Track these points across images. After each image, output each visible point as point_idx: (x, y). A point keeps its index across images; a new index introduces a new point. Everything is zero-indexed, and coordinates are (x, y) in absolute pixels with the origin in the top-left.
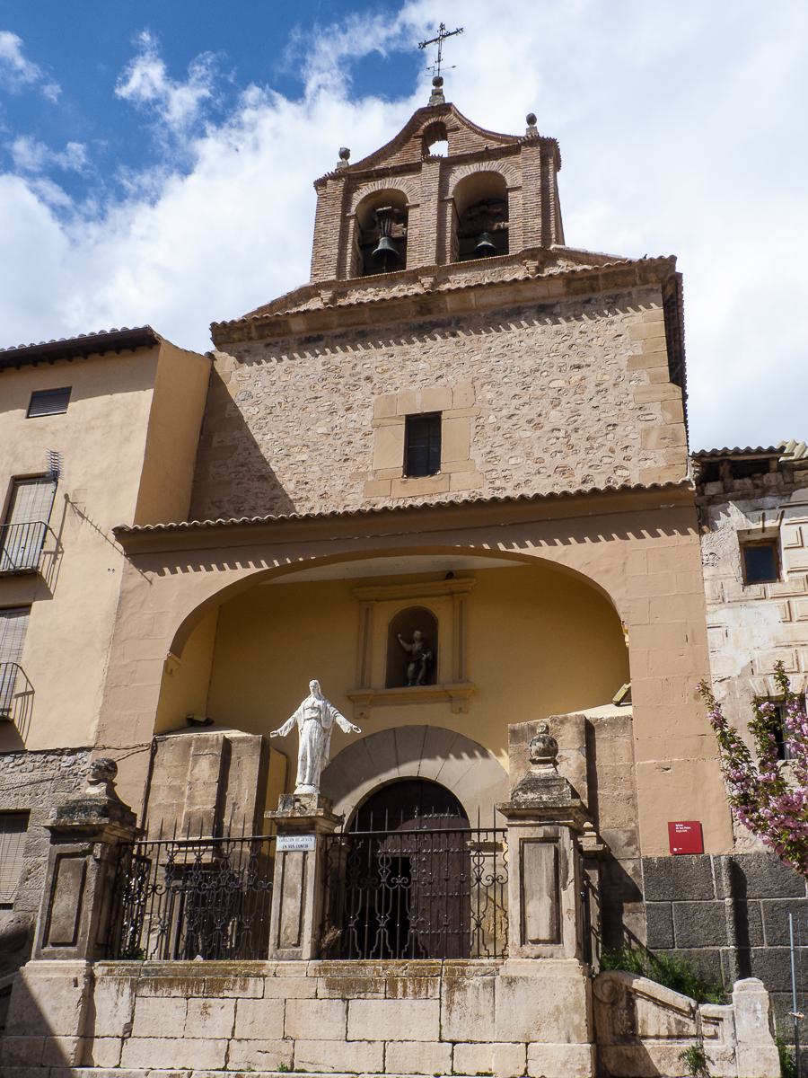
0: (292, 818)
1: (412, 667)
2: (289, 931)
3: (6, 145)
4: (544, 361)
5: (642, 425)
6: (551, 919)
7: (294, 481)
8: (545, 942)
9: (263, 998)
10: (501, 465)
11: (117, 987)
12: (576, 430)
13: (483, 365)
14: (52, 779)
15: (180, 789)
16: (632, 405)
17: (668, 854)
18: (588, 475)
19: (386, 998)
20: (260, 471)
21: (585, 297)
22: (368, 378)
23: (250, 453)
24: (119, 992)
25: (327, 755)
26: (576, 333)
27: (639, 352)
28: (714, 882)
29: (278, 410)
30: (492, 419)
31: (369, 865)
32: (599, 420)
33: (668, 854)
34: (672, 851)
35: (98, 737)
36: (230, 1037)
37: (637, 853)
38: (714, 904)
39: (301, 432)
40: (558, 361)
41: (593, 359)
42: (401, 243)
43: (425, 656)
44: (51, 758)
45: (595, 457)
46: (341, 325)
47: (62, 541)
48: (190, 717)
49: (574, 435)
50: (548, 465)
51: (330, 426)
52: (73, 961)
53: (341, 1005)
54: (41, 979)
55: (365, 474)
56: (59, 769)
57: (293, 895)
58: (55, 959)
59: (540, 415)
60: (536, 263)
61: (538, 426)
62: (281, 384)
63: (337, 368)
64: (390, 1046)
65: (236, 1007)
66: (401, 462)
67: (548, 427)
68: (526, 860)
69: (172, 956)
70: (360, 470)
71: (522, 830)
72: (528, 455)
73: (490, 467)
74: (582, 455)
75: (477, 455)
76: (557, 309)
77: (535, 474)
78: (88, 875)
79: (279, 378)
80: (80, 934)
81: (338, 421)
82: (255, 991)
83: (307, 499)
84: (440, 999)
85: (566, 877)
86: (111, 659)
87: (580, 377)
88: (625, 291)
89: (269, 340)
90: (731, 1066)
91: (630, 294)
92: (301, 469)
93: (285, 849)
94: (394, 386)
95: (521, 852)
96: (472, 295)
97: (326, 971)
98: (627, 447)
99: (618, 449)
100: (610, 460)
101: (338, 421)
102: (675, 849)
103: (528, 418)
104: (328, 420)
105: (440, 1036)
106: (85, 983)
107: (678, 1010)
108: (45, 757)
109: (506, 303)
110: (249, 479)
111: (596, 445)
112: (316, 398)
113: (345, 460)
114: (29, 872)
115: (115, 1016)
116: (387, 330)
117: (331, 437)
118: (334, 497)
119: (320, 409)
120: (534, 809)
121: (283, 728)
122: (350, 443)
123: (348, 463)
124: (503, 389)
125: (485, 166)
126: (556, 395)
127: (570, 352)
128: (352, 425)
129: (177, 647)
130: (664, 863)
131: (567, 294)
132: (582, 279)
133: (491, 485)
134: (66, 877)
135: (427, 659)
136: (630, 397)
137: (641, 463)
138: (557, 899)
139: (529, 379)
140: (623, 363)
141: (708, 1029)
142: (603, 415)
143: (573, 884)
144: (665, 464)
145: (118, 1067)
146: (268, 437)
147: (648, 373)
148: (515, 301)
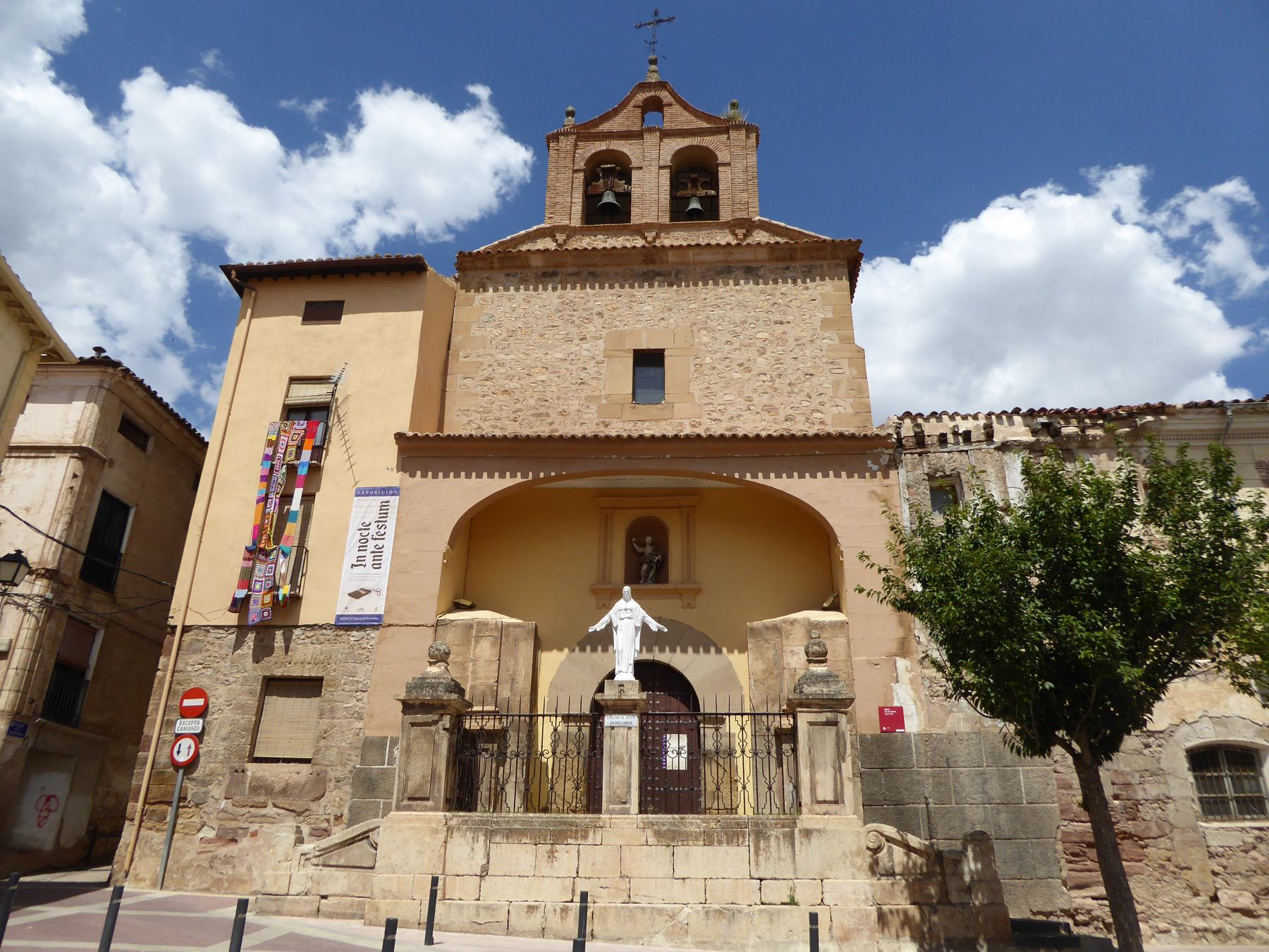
1: (645, 567)
7: (535, 398)
11: (472, 835)
16: (824, 360)
20: (504, 386)
21: (785, 264)
22: (600, 314)
24: (475, 840)
27: (830, 315)
30: (708, 360)
33: (878, 732)
34: (881, 728)
36: (575, 875)
40: (762, 316)
42: (625, 197)
45: (796, 399)
46: (574, 265)
49: (777, 380)
55: (599, 397)
57: (620, 762)
60: (744, 231)
61: (748, 370)
63: (571, 302)
64: (709, 882)
65: (578, 852)
73: (706, 400)
75: (696, 389)
76: (761, 272)
82: (594, 839)
83: (547, 415)
87: (781, 331)
88: (818, 263)
91: (821, 266)
96: (691, 252)
99: (814, 395)
100: (808, 404)
109: (719, 262)
112: (554, 326)
116: (616, 273)
119: (557, 337)
124: (717, 335)
125: (695, 141)
129: (452, 542)
130: (876, 740)
131: (770, 260)
132: (783, 250)
133: (709, 417)
135: (658, 560)
136: (824, 353)
143: (850, 758)
145: (478, 900)
148: (726, 261)
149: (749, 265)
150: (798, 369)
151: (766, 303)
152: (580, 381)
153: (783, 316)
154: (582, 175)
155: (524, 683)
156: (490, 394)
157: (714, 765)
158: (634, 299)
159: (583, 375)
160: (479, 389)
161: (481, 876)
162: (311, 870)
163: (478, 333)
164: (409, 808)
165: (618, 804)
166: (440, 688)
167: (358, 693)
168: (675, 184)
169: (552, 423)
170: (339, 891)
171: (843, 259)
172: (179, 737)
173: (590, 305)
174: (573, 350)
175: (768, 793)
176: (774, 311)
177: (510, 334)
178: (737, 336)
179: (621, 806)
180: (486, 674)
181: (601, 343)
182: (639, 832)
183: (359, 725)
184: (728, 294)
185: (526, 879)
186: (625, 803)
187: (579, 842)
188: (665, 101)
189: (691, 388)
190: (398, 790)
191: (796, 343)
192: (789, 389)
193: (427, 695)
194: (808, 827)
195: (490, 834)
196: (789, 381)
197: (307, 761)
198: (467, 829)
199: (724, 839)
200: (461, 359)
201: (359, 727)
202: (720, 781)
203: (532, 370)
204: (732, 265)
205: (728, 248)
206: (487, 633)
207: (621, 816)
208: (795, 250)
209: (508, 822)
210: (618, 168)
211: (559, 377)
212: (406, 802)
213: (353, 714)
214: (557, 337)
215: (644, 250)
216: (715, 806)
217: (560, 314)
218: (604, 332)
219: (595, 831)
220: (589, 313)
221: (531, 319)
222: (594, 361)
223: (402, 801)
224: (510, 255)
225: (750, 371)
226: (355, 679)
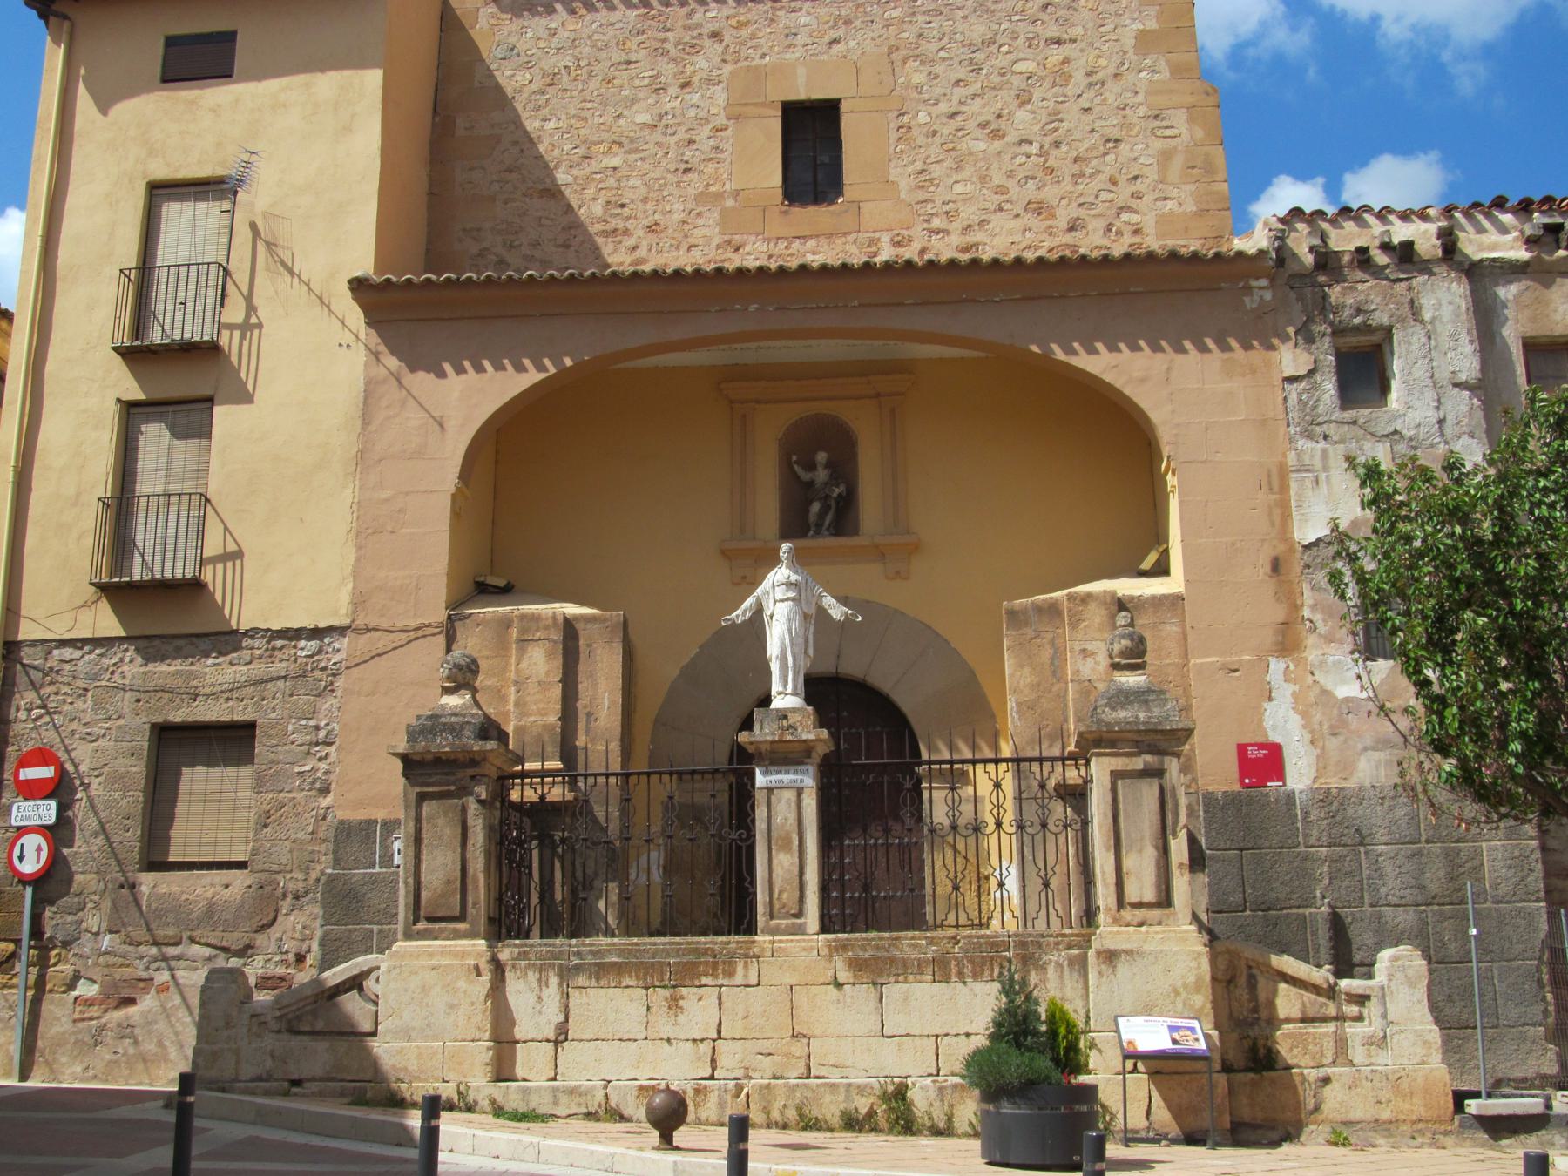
0: (780, 741)
1: (816, 507)
2: (785, 896)
3: (1320, 180)
4: (1003, 27)
5: (1158, 144)
6: (1158, 876)
8: (1149, 905)
10: (941, 194)
11: (537, 975)
12: (1057, 144)
13: (905, 26)
14: (285, 677)
15: (499, 691)
16: (1142, 111)
17: (1237, 787)
18: (1078, 219)
22: (715, 35)
23: (522, 151)
24: (543, 983)
25: (811, 652)
27: (1152, 24)
28: (1300, 825)
29: (565, 80)
32: (1092, 131)
33: (1237, 787)
34: (1242, 783)
35: (355, 612)
37: (1193, 785)
38: (1299, 853)
39: (608, 119)
40: (1024, 29)
41: (1080, 30)
44: (279, 643)
45: (1088, 188)
47: (256, 301)
48: (482, 579)
49: (1054, 152)
50: (1014, 198)
51: (656, 111)
53: (873, 993)
54: (423, 966)
55: (719, 196)
56: (295, 661)
57: (786, 846)
58: (436, 939)
59: (999, 116)
61: (996, 134)
62: (566, 34)
64: (944, 1042)
65: (720, 998)
66: (777, 179)
67: (1012, 137)
68: (1121, 798)
70: (712, 189)
71: (1113, 760)
72: (983, 179)
73: (922, 195)
74: (1067, 185)
75: (902, 176)
77: (995, 211)
78: (470, 822)
79: (563, 24)
80: (470, 904)
81: (668, 103)
82: (746, 976)
83: (626, 232)
85: (1176, 822)
86: (360, 488)
87: (1061, 58)
90: (1380, 1051)
92: (611, 182)
94: (760, 52)
95: (1114, 790)
97: (845, 948)
98: (1136, 178)
99: (1122, 180)
101: (668, 103)
102: (1247, 781)
103: (981, 119)
104: (651, 101)
106: (490, 971)
107: (1315, 989)
108: (269, 642)
110: (524, 195)
111: (1088, 171)
112: (629, 63)
113: (686, 171)
114: (268, 814)
115: (540, 1013)
117: (659, 131)
118: (670, 231)
119: (637, 82)
120: (1129, 731)
121: (739, 611)
122: (691, 142)
123: (690, 176)
124: (939, 69)
126: (1024, 86)
127: (1044, 16)
128: (692, 113)
130: (1232, 800)
134: (435, 825)
135: (840, 495)
136: (1140, 98)
137: (1158, 203)
138: (1164, 851)
139: (979, 56)
140: (1129, 42)
141: (1350, 1010)
142: (1098, 124)
144: (1195, 209)
145: (554, 1079)
146: (552, 124)
147: (1168, 62)
157: (949, 852)
159: (688, 154)
160: (496, 187)
162: (269, 1041)
164: (423, 935)
169: (635, 248)
170: (319, 1072)
172: (22, 831)
175: (1043, 894)
180: (541, 706)
182: (822, 963)
187: (720, 982)
190: (406, 905)
192: (1076, 169)
193: (443, 744)
195: (566, 974)
197: (241, 865)
198: (528, 966)
199: (968, 970)
203: (594, 148)
206: (538, 635)
218: (728, 69)
219: (746, 963)
225: (1004, 136)
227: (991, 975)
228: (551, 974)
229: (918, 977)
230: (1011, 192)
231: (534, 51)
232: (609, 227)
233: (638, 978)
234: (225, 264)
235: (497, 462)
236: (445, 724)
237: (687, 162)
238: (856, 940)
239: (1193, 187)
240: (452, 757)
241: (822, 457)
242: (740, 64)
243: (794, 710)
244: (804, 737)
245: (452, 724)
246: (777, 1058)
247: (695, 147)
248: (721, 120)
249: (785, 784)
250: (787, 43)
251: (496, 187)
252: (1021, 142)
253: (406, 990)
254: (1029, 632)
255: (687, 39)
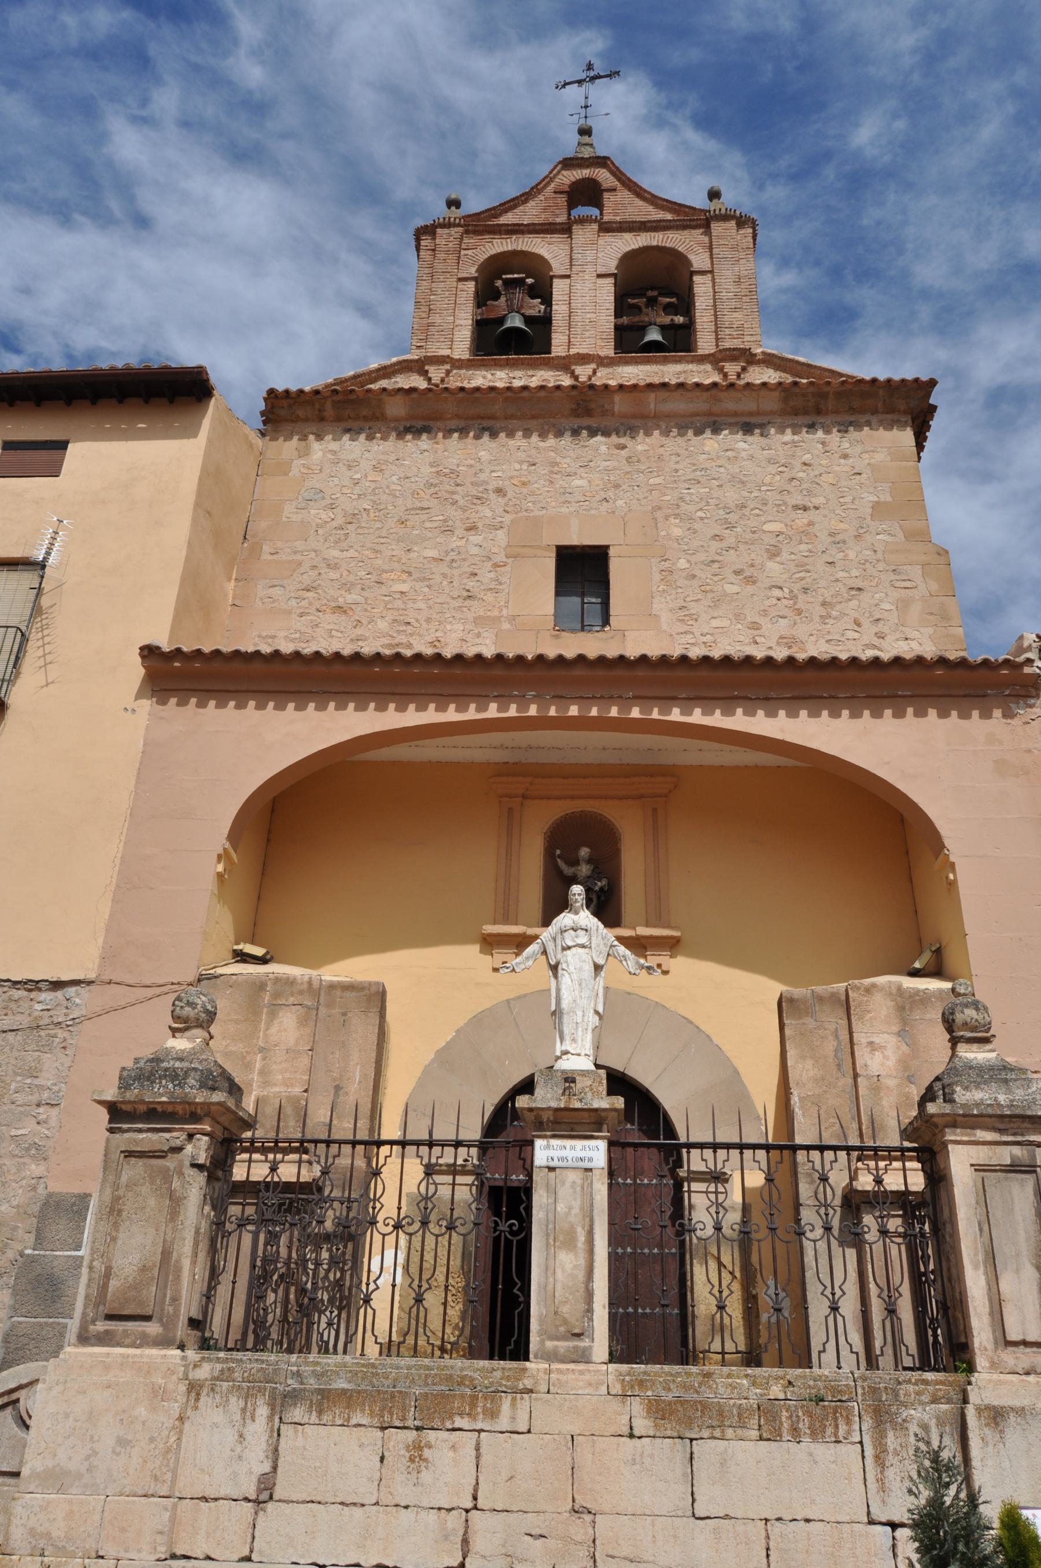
4: (753, 495)
9: (529, 1432)
11: (242, 1403)
13: (668, 492)
15: (244, 1057)
19: (761, 1439)
20: (336, 600)
22: (499, 491)
24: (248, 1414)
26: (797, 464)
27: (886, 498)
31: (505, 1197)
36: (469, 1504)
40: (772, 497)
42: (543, 323)
43: (599, 884)
46: (458, 416)
49: (802, 597)
52: (154, 1352)
55: (498, 619)
57: (570, 1243)
61: (751, 580)
63: (452, 471)
65: (478, 1448)
69: (331, 1350)
82: (513, 1418)
84: (861, 1443)
86: (125, 843)
87: (806, 521)
89: (350, 424)
93: (552, 1164)
96: (652, 396)
99: (866, 622)
100: (856, 635)
101: (455, 542)
105: (869, 1513)
109: (698, 414)
111: (834, 613)
112: (423, 509)
115: (240, 1457)
119: (428, 525)
120: (990, 1116)
124: (697, 526)
129: (235, 835)
131: (783, 413)
132: (804, 395)
135: (601, 889)
149: (747, 420)
150: (837, 580)
151: (778, 478)
152: (465, 594)
153: (807, 499)
154: (471, 286)
155: (357, 1091)
156: (313, 610)
157: (713, 1265)
158: (556, 469)
159: (471, 584)
160: (293, 602)
161: (257, 1502)
163: (296, 518)
164: (105, 1339)
165: (563, 1338)
166: (191, 1081)
167: (41, 1110)
168: (621, 307)
171: (905, 413)
173: (483, 477)
174: (454, 545)
175: (831, 1319)
176: (792, 490)
177: (349, 520)
178: (731, 528)
179: (571, 1344)
180: (287, 1075)
181: (501, 534)
182: (615, 1404)
183: (35, 1169)
184: (714, 464)
185: (358, 1512)
186: (578, 1335)
187: (479, 1426)
188: (605, 186)
189: (654, 606)
190: (87, 1297)
191: (833, 539)
193: (160, 1094)
194: (996, 1403)
196: (821, 599)
198: (230, 1391)
199: (804, 1426)
200: (266, 556)
201: (37, 1174)
202: (838, 1293)
203: (384, 576)
204: (719, 419)
205: (714, 391)
206: (291, 1000)
207: (572, 1366)
208: (824, 396)
209: (323, 1374)
210: (530, 281)
211: (429, 587)
212: (101, 1326)
213: (28, 1149)
214: (428, 525)
215: (574, 393)
216: (716, 1346)
217: (433, 490)
218: (507, 519)
219: (514, 1399)
220: (481, 489)
221: (384, 497)
222: (490, 563)
223: (93, 1322)
224: (353, 397)
226: (36, 1082)
227: (836, 1435)
228: (260, 1401)
229: (739, 1431)
230: (764, 628)
231: (338, 495)
232: (396, 641)
233: (372, 1414)
234: (24, 629)
235: (268, 840)
236: (166, 1069)
237: (468, 591)
238: (656, 1374)
239: (931, 630)
240: (170, 1109)
241: (584, 852)
242: (520, 515)
243: (584, 1073)
244: (596, 1104)
245: (174, 1070)
246: (550, 1543)
247: (477, 578)
248: (500, 558)
249: (570, 1164)
250: (563, 499)
251: (293, 602)
252: (770, 588)
253: (67, 1416)
254: (810, 1022)
255: (475, 493)
